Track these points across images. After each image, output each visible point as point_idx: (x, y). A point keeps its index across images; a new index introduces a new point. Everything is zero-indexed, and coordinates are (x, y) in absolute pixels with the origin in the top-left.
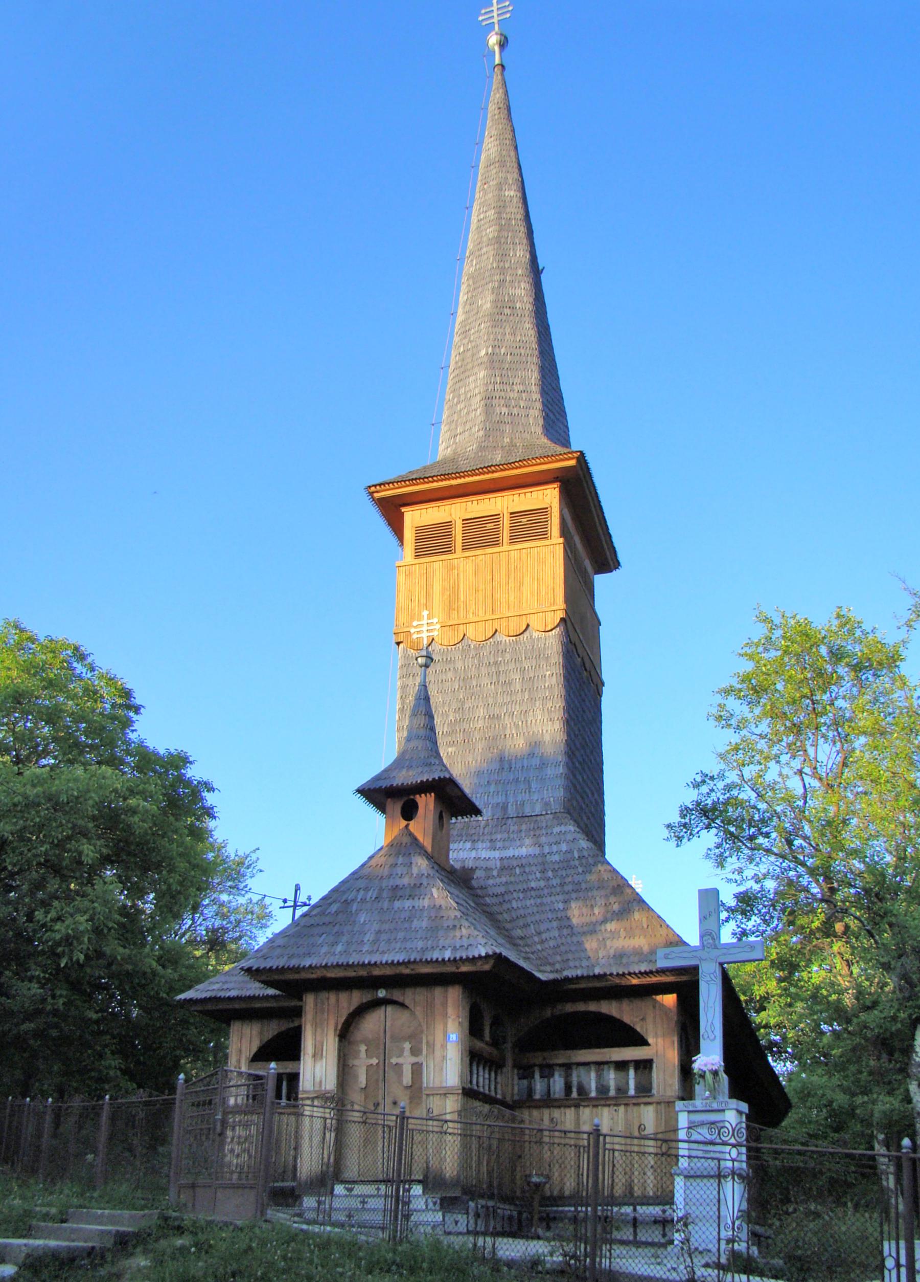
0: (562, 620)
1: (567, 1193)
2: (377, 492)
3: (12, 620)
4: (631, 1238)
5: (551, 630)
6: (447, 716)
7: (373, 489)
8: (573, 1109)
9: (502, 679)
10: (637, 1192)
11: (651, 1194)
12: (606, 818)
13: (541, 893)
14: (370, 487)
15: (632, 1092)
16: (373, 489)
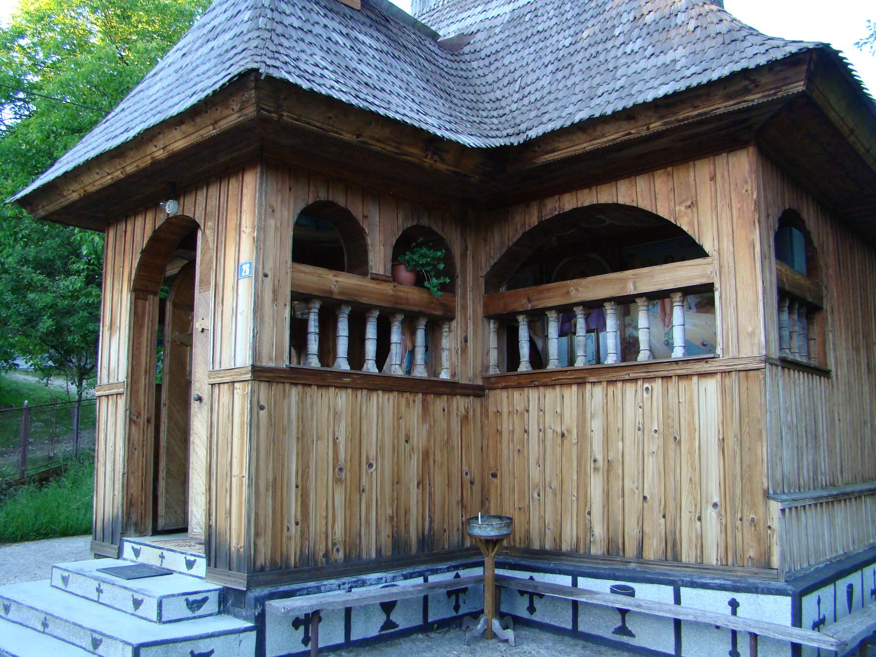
1: (565, 547)
4: (569, 626)
8: (574, 388)
10: (688, 555)
11: (714, 562)
13: (547, 34)
15: (678, 353)
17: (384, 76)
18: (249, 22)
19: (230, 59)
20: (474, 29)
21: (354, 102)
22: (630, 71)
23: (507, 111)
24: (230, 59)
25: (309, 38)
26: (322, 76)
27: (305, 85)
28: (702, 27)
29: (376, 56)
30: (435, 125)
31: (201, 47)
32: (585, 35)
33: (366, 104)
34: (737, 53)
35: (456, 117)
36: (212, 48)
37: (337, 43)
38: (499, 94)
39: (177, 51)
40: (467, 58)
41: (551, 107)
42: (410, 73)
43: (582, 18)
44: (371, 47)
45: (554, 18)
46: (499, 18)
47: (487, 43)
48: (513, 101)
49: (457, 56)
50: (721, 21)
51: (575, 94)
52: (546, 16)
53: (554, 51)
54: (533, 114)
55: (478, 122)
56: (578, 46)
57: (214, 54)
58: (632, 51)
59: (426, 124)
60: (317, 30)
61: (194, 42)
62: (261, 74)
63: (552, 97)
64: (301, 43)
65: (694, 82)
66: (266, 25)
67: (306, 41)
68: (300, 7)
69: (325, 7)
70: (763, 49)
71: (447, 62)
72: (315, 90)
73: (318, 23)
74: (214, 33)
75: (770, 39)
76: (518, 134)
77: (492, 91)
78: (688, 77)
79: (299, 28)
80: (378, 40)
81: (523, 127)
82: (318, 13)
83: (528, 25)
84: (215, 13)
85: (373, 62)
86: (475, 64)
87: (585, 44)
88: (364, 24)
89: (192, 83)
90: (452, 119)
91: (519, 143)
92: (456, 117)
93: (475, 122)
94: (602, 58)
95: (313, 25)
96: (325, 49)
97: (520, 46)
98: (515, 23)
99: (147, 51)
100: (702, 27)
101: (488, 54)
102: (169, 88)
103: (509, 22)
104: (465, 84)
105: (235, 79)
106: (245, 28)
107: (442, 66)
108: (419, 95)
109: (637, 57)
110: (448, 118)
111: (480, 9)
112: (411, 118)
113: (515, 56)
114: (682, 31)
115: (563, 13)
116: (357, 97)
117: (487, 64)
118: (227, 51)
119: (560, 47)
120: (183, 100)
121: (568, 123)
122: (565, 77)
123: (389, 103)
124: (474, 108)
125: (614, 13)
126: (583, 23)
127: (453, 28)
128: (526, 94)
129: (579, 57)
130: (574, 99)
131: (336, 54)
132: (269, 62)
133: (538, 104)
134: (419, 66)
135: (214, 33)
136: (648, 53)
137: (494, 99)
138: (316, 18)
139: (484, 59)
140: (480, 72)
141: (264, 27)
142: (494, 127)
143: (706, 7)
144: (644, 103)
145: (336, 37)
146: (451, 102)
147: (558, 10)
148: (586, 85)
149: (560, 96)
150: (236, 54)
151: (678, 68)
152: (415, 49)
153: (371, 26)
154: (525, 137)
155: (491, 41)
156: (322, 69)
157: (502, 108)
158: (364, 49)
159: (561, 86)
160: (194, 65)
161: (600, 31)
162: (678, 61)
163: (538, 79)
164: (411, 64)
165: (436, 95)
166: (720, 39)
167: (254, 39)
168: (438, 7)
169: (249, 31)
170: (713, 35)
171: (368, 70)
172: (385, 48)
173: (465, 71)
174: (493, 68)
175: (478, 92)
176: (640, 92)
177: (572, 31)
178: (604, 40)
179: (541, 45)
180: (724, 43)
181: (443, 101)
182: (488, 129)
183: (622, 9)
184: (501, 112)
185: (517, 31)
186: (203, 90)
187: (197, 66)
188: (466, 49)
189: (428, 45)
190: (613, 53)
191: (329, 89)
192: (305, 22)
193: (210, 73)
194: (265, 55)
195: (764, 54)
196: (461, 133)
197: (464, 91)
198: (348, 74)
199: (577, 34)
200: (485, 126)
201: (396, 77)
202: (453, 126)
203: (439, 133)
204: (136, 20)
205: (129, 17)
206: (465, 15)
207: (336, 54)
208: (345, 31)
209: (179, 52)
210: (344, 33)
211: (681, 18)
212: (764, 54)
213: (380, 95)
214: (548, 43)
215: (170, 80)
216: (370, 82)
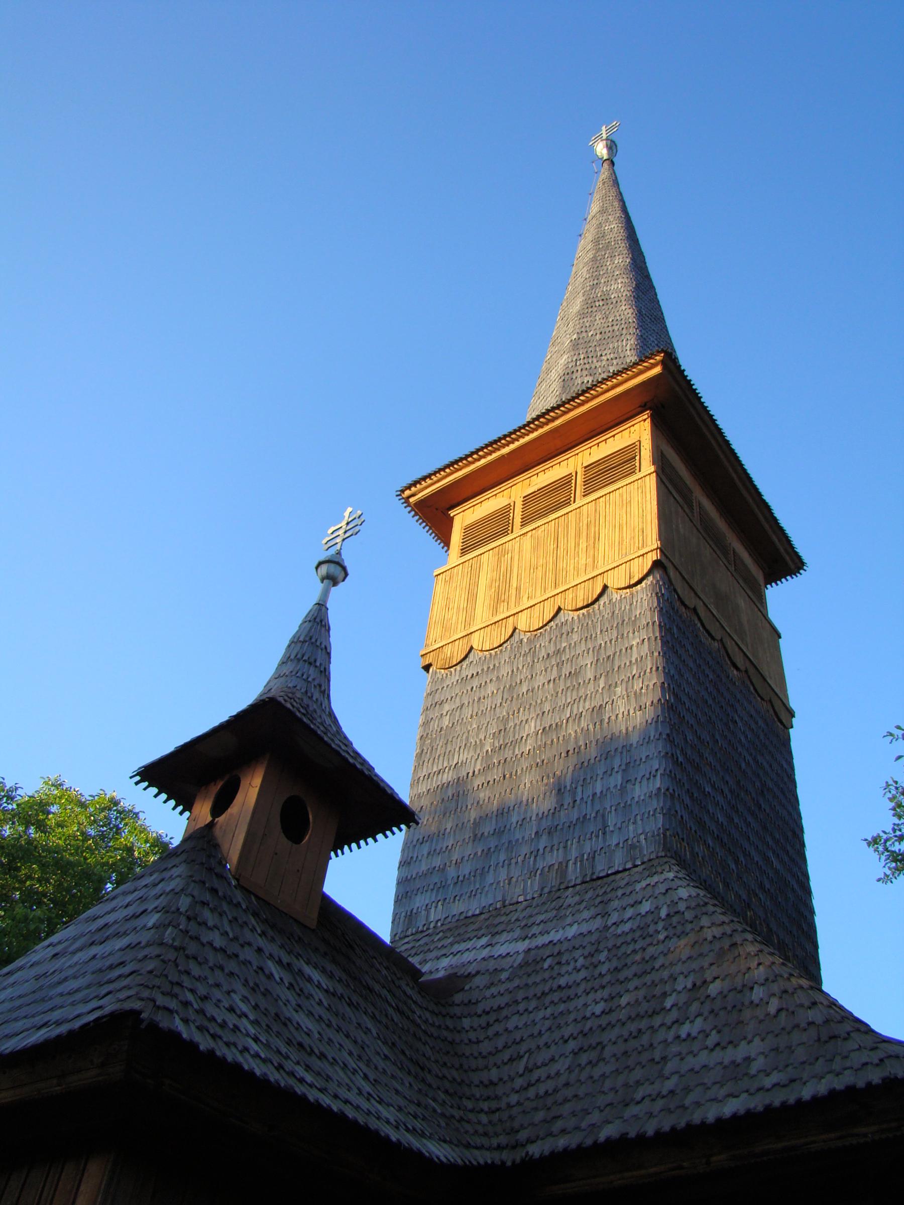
0: (656, 564)
2: (413, 495)
3: (53, 778)
5: (640, 582)
6: (482, 745)
7: (407, 493)
9: (566, 670)
12: (817, 919)
13: (571, 992)
14: (403, 491)
16: (407, 493)
17: (330, 1033)
18: (152, 931)
19: (110, 982)
20: (472, 969)
21: (274, 1076)
22: (684, 1068)
23: (503, 1105)
24: (110, 982)
25: (232, 966)
26: (236, 1028)
27: (204, 1043)
28: (787, 1010)
29: (324, 1000)
30: (392, 1120)
31: (80, 949)
32: (624, 1001)
33: (291, 1081)
34: (838, 1059)
35: (426, 1108)
36: (94, 957)
37: (270, 976)
38: (494, 1074)
39: (49, 946)
40: (457, 1011)
41: (567, 1108)
42: (369, 1030)
43: (622, 976)
44: (319, 986)
45: (583, 970)
46: (509, 959)
47: (488, 993)
48: (513, 1089)
49: (444, 1006)
50: (814, 1004)
51: (603, 1092)
52: (572, 964)
53: (579, 1019)
54: (540, 1115)
55: (457, 1117)
56: (613, 1017)
57: (96, 965)
58: (689, 1035)
59: (379, 1118)
60: (247, 954)
61: (75, 939)
62: (142, 1021)
63: (569, 1092)
64: (218, 972)
65: (777, 1099)
66: (174, 939)
67: (226, 971)
68: (230, 918)
69: (266, 921)
70: (875, 1057)
71: (428, 1015)
72: (218, 1053)
73: (249, 944)
74: (104, 934)
75: (884, 1041)
76: (514, 1147)
77: (486, 1067)
78: (768, 1090)
79: (221, 948)
80: (331, 976)
81: (523, 1135)
82: (253, 930)
83: (546, 975)
84: (113, 904)
85: (318, 1010)
86: (466, 1023)
87: (623, 1015)
88: (316, 950)
89: (49, 1005)
90: (419, 1111)
91: (514, 1162)
92: (426, 1108)
93: (453, 1117)
94: (645, 1039)
95: (242, 946)
96: (251, 984)
97: (533, 1004)
98: (529, 969)
99: (26, 919)
100: (787, 1010)
101: (488, 1009)
102: (18, 1003)
103: (521, 966)
104: (448, 1052)
105: (104, 1020)
106: (145, 937)
107: (419, 1021)
108: (376, 1068)
109: (695, 1047)
110: (412, 1109)
111: (484, 941)
112: (357, 1108)
113: (524, 1019)
114: (760, 1013)
115: (596, 963)
116: (280, 1067)
117: (484, 1024)
118: (111, 967)
119: (588, 1014)
120: (27, 1030)
121: (589, 1142)
122: (590, 1062)
123: (328, 1078)
124: (455, 1093)
125: (665, 974)
126: (622, 982)
127: (445, 962)
128: (533, 1082)
129: (613, 1034)
130: (601, 1100)
131: (266, 993)
132: (161, 1000)
133: (549, 1101)
134: (384, 1020)
135: (104, 934)
136: (710, 1042)
137: (486, 1082)
138: (248, 935)
139: (480, 1016)
140: (472, 1036)
141: (171, 942)
142: (481, 1130)
143: (794, 980)
144: (703, 1123)
145: (271, 967)
146: (423, 1080)
147: (589, 958)
148: (621, 1079)
149: (581, 1093)
150: (120, 976)
151: (753, 1071)
152: (384, 992)
153: (326, 954)
154: (524, 1155)
155: (494, 990)
156: (240, 1017)
157: (497, 1098)
158: (309, 988)
159: (584, 1076)
160: (63, 975)
161: (645, 998)
162: (755, 1059)
163: (552, 1059)
164: (373, 1017)
165: (401, 1069)
166: (813, 1032)
167: (151, 958)
168: (428, 929)
169: (148, 945)
170: (803, 1025)
171: (307, 1023)
172: (340, 990)
173: (451, 1031)
174: (490, 1032)
175: (466, 1067)
176: (698, 1104)
177: (605, 993)
178: (650, 1013)
179: (562, 1007)
180: (819, 1040)
181: (411, 1079)
182: (472, 1131)
183: (678, 968)
184: (494, 1105)
185: (530, 982)
186: (58, 1023)
187: (66, 979)
188: (458, 998)
189: (404, 987)
190: (661, 1035)
191: (241, 1052)
192: (232, 940)
193: (79, 996)
194: (159, 987)
195: (877, 1065)
196: (430, 1138)
197: (445, 1064)
198: (275, 1027)
199: (613, 998)
200: (468, 1127)
201: (347, 1036)
202: (418, 1125)
203: (394, 1136)
204: (25, 874)
205: (18, 869)
206: (463, 946)
207: (266, 993)
208: (286, 959)
209: (51, 948)
210: (285, 963)
211: (758, 993)
212: (877, 1065)
213: (317, 1064)
214: (571, 1005)
215: (27, 987)
216: (306, 1041)
